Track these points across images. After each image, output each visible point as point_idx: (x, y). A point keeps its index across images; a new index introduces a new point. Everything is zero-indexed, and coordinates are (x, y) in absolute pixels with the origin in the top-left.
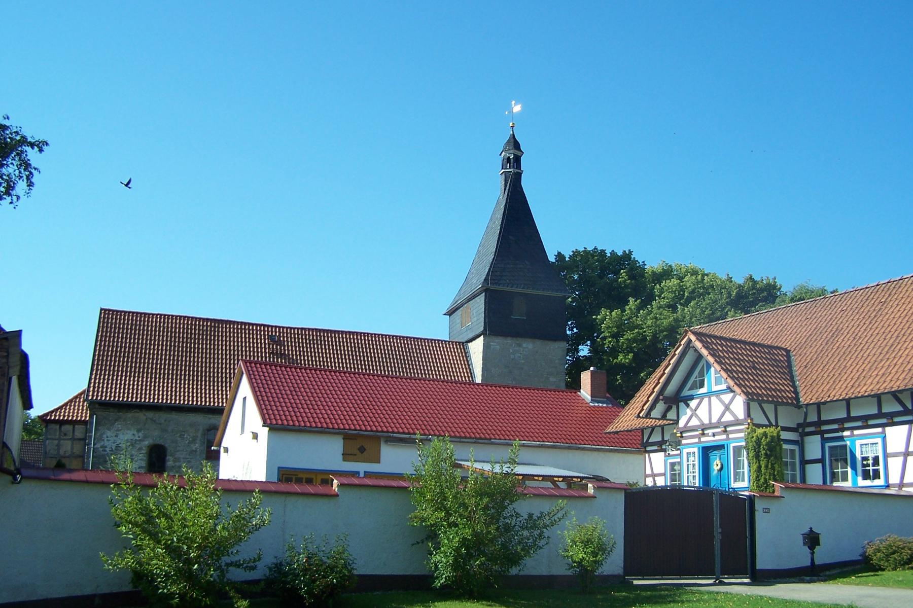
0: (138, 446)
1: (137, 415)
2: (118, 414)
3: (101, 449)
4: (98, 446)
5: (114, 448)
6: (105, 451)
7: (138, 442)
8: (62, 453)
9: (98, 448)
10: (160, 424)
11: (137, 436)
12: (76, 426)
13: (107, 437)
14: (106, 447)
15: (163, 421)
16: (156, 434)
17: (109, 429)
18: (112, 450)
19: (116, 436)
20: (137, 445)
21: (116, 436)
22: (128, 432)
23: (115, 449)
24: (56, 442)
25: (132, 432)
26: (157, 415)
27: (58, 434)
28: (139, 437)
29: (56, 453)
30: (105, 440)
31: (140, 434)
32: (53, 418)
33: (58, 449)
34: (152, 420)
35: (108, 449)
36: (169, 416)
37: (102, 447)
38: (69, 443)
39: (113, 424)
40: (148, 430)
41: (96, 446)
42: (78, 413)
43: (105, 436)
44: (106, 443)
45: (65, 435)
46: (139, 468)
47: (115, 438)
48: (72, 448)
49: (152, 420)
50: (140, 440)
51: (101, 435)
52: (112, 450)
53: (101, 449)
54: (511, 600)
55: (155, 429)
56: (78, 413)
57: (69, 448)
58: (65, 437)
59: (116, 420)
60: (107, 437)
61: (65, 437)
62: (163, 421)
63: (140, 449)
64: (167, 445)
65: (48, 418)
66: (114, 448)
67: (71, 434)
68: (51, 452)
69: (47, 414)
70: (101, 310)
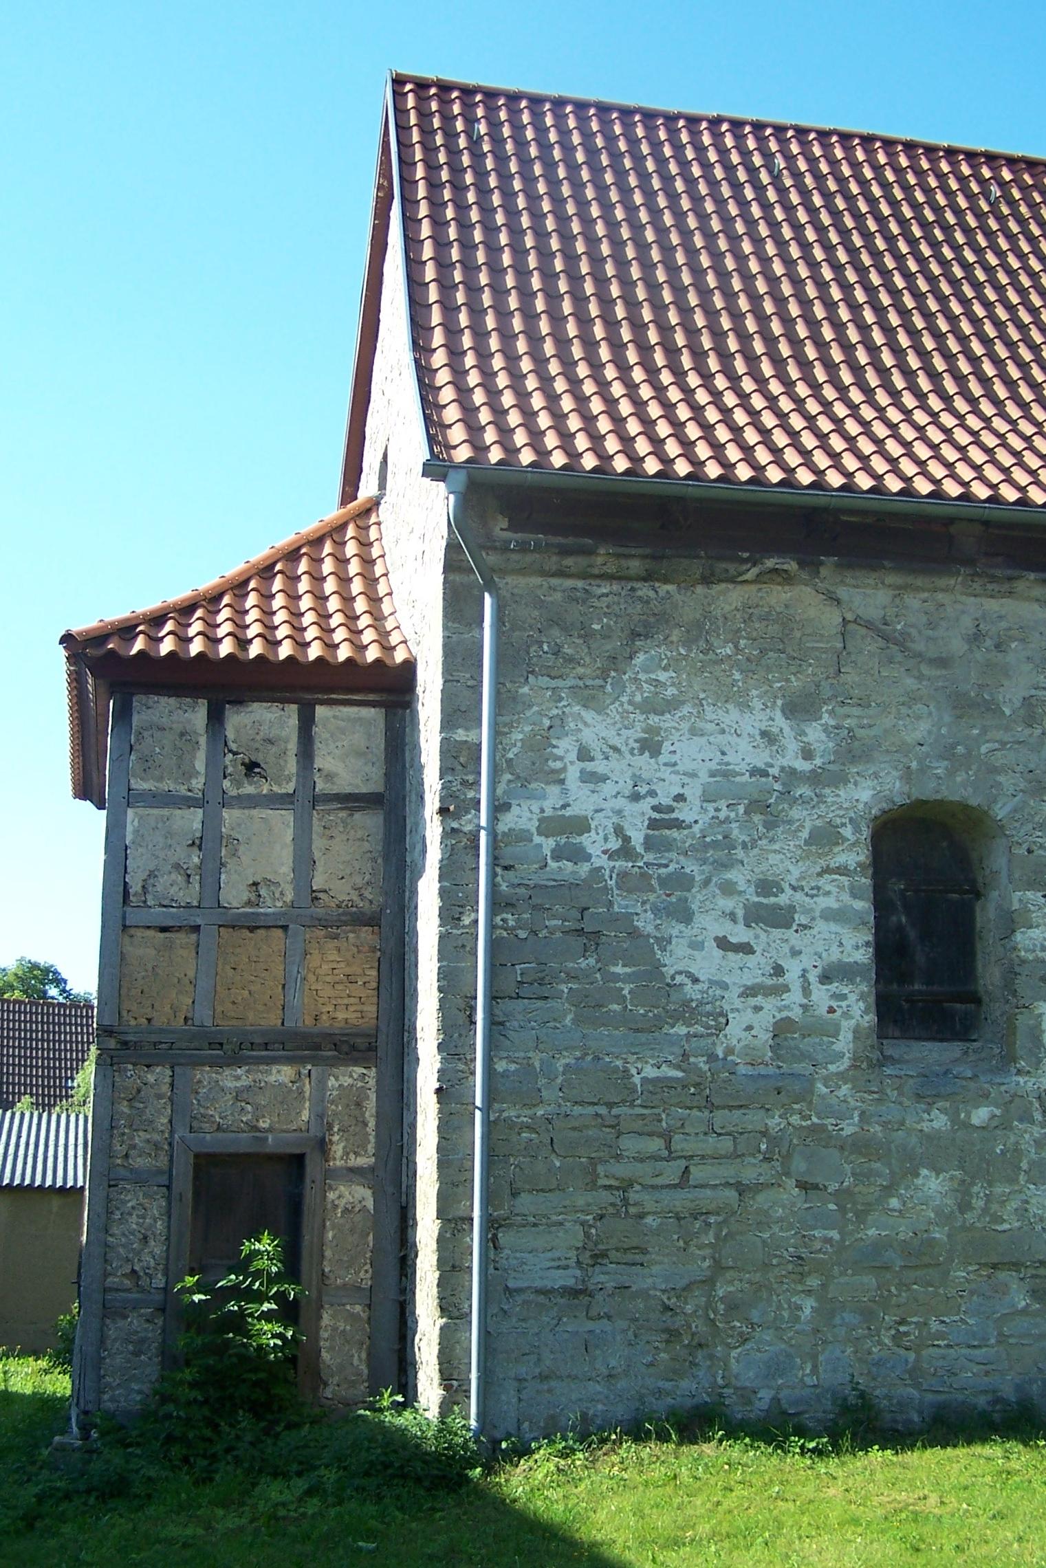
0: (805, 818)
1: (778, 596)
2: (644, 590)
3: (548, 844)
4: (522, 817)
5: (637, 838)
6: (579, 855)
7: (803, 790)
8: (234, 894)
9: (523, 836)
10: (942, 662)
11: (792, 747)
12: (321, 711)
13: (584, 754)
14: (581, 825)
15: (957, 646)
16: (922, 729)
17: (590, 698)
18: (626, 851)
19: (650, 745)
20: (796, 813)
21: (650, 745)
22: (731, 716)
23: (649, 844)
24: (193, 820)
25: (752, 722)
26: (913, 601)
27: (200, 765)
28: (807, 754)
29: (191, 894)
30: (573, 773)
31: (815, 734)
32: (166, 647)
33: (210, 873)
34: (880, 630)
35: (595, 844)
36: (992, 605)
37: (548, 826)
38: (283, 822)
39: (615, 663)
40: (863, 704)
41: (508, 822)
42: (559, 418)
43: (565, 747)
44: (582, 801)
45: (251, 767)
46: (825, 978)
47: (644, 762)
48: (304, 862)
49: (880, 630)
50: (814, 778)
51: (541, 744)
52: (626, 851)
53: (548, 844)
54: (197, 1298)
55: (912, 699)
56: (559, 418)
57: (281, 864)
58: (249, 789)
59: (638, 634)
60: (584, 754)
61: (249, 789)
62: (957, 646)
63: (826, 837)
64: (1001, 811)
65: (139, 645)
66: (637, 838)
67: (292, 766)
68: (162, 882)
69: (126, 630)
70: (398, 81)
